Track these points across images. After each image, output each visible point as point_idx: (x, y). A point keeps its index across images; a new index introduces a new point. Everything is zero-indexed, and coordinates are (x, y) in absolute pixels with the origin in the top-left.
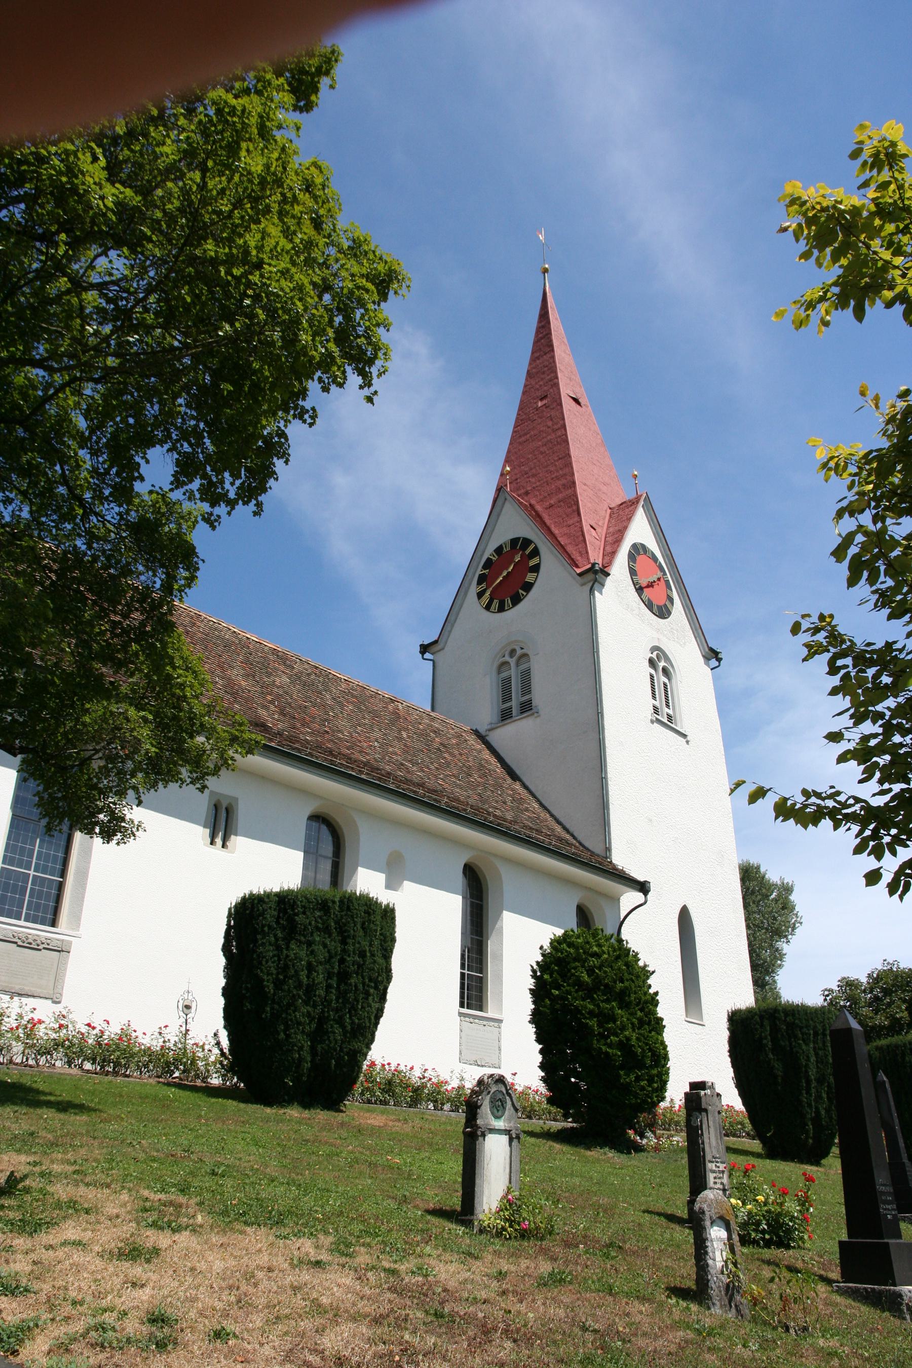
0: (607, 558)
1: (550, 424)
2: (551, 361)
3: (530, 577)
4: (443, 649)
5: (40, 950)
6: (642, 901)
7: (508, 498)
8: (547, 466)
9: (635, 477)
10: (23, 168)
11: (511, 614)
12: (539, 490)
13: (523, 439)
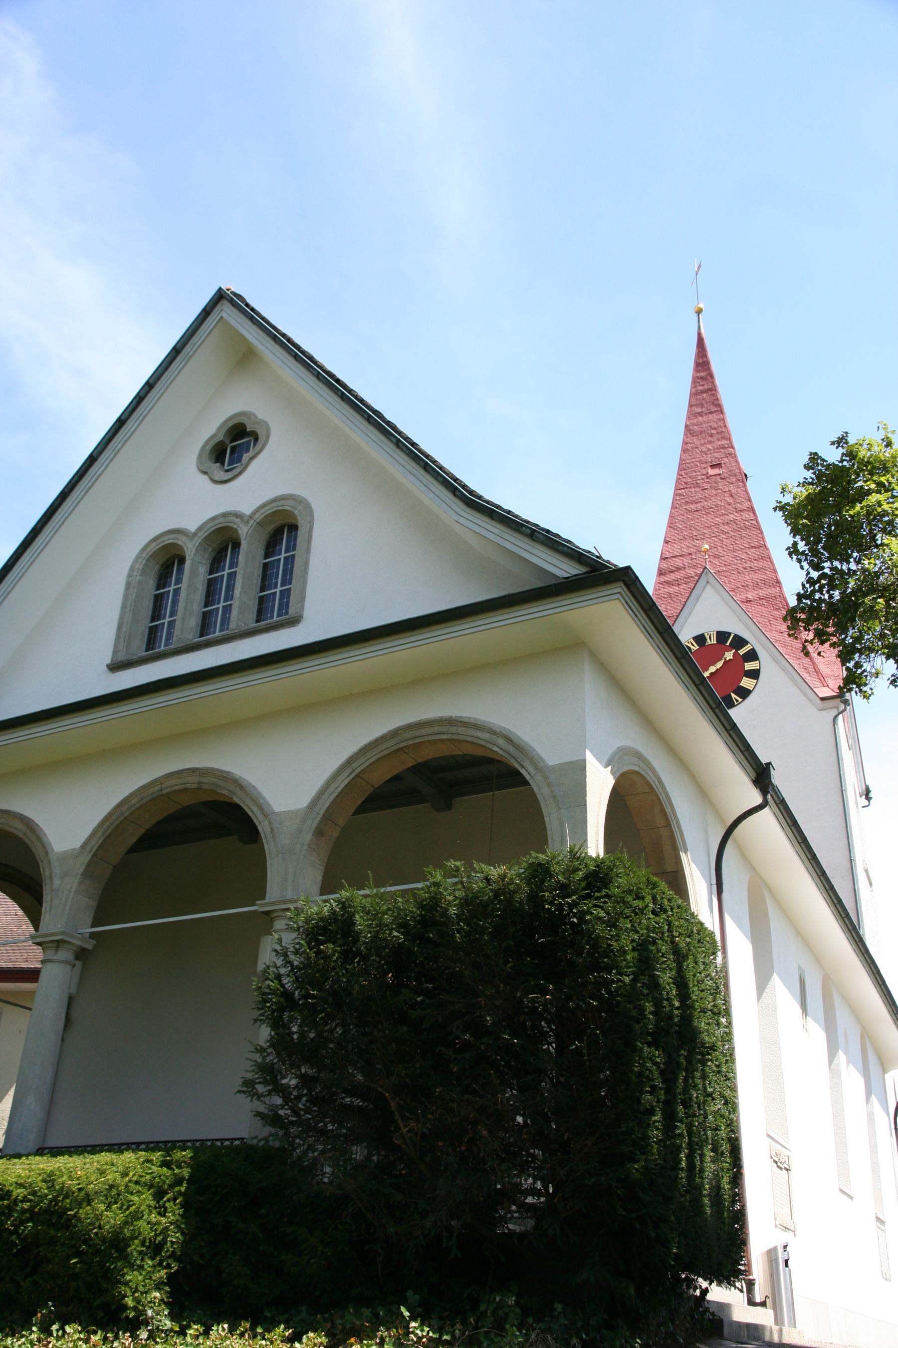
0: (528, 531)
1: (730, 500)
2: (721, 424)
3: (746, 683)
7: (711, 579)
8: (734, 551)
10: (187, 1289)
13: (692, 507)
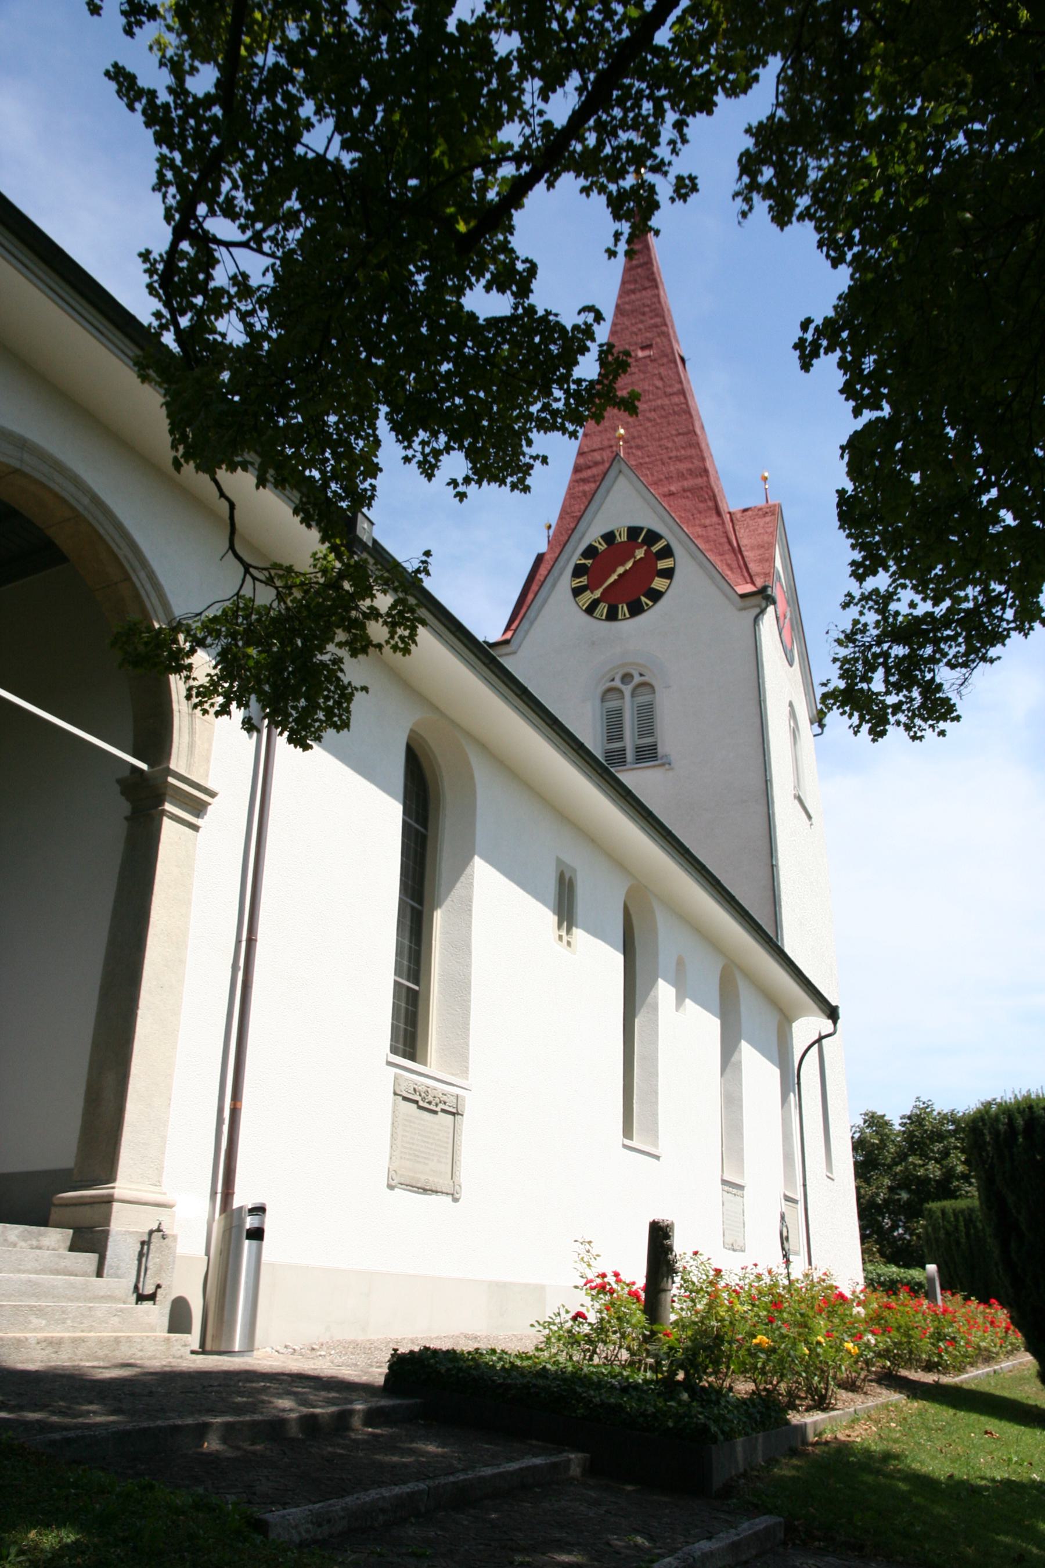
1: (659, 384)
2: (655, 300)
3: (658, 584)
4: (514, 653)
5: (435, 1112)
6: (831, 1030)
8: (660, 439)
9: (765, 479)
11: (628, 627)
12: (649, 469)
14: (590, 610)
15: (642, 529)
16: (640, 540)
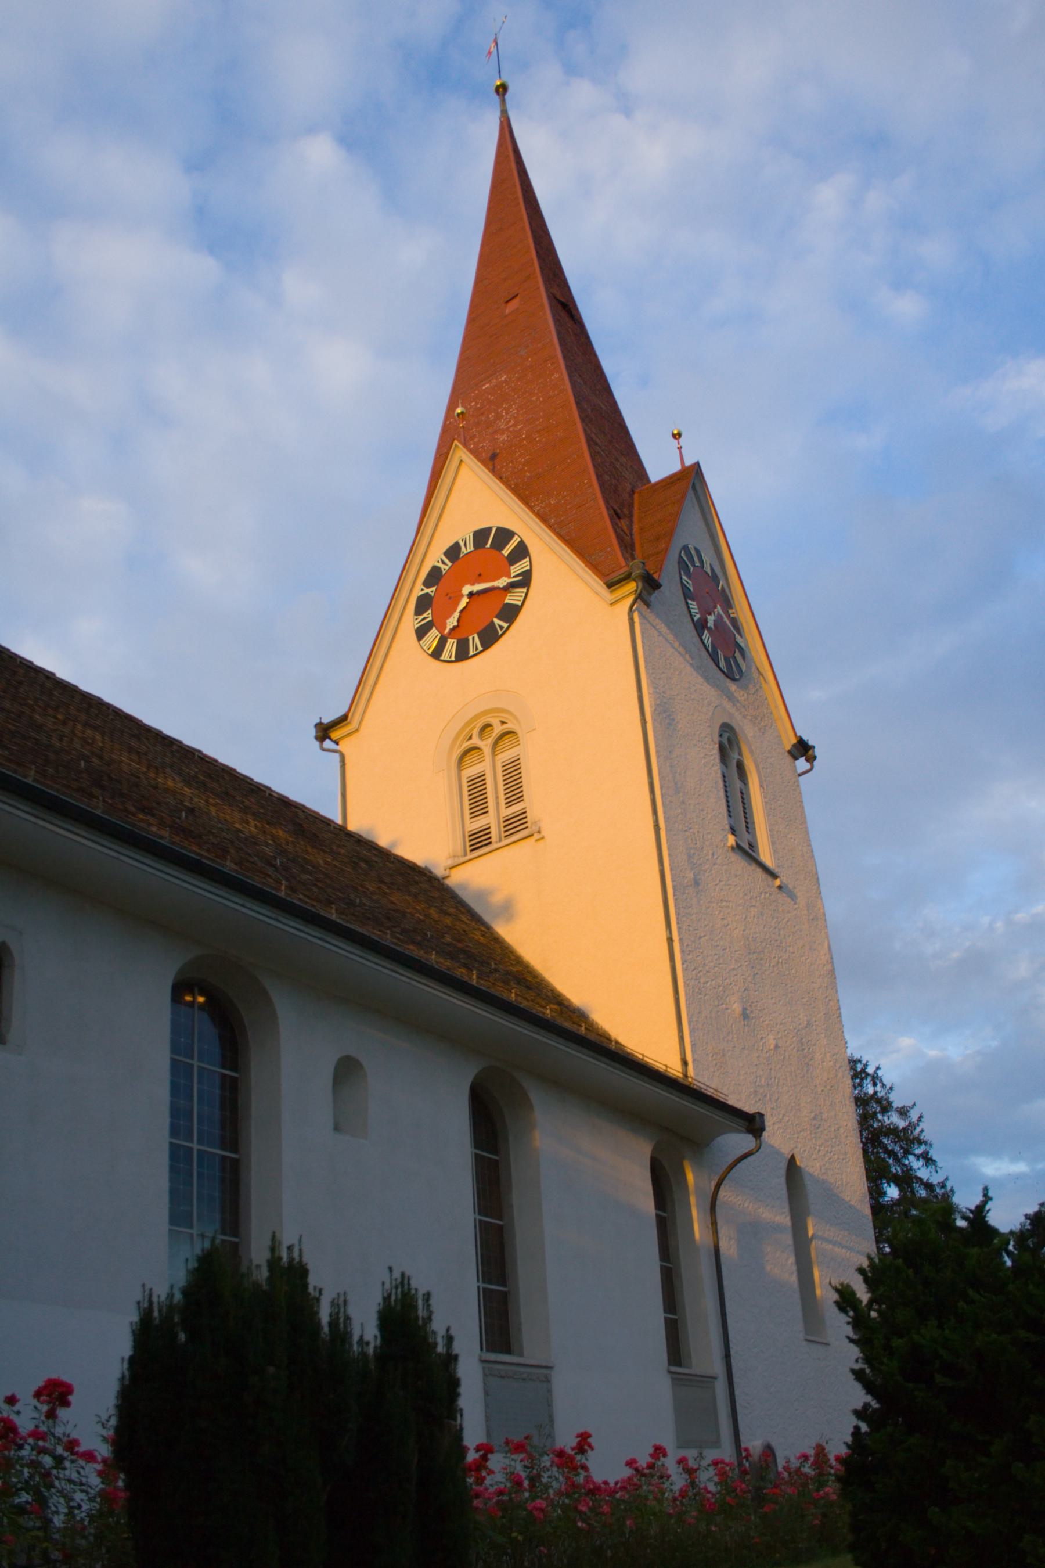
4: (357, 731)
11: (485, 665)
14: (437, 654)
15: (490, 529)
16: (488, 546)
